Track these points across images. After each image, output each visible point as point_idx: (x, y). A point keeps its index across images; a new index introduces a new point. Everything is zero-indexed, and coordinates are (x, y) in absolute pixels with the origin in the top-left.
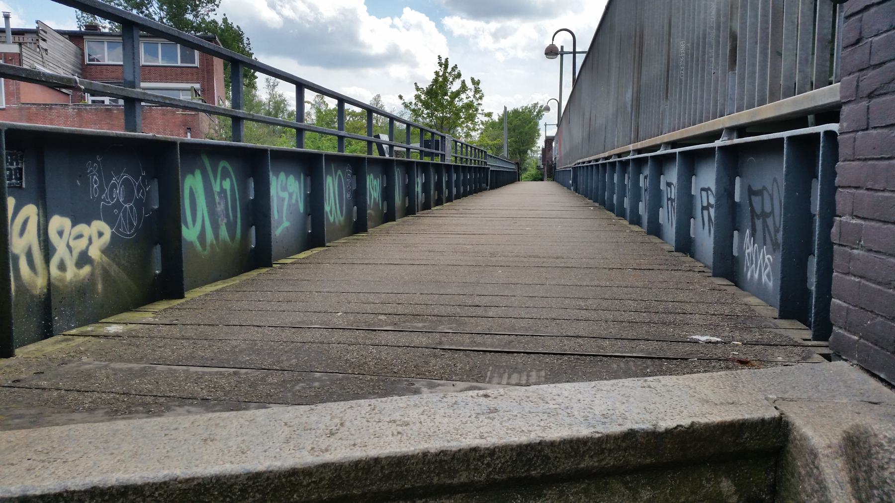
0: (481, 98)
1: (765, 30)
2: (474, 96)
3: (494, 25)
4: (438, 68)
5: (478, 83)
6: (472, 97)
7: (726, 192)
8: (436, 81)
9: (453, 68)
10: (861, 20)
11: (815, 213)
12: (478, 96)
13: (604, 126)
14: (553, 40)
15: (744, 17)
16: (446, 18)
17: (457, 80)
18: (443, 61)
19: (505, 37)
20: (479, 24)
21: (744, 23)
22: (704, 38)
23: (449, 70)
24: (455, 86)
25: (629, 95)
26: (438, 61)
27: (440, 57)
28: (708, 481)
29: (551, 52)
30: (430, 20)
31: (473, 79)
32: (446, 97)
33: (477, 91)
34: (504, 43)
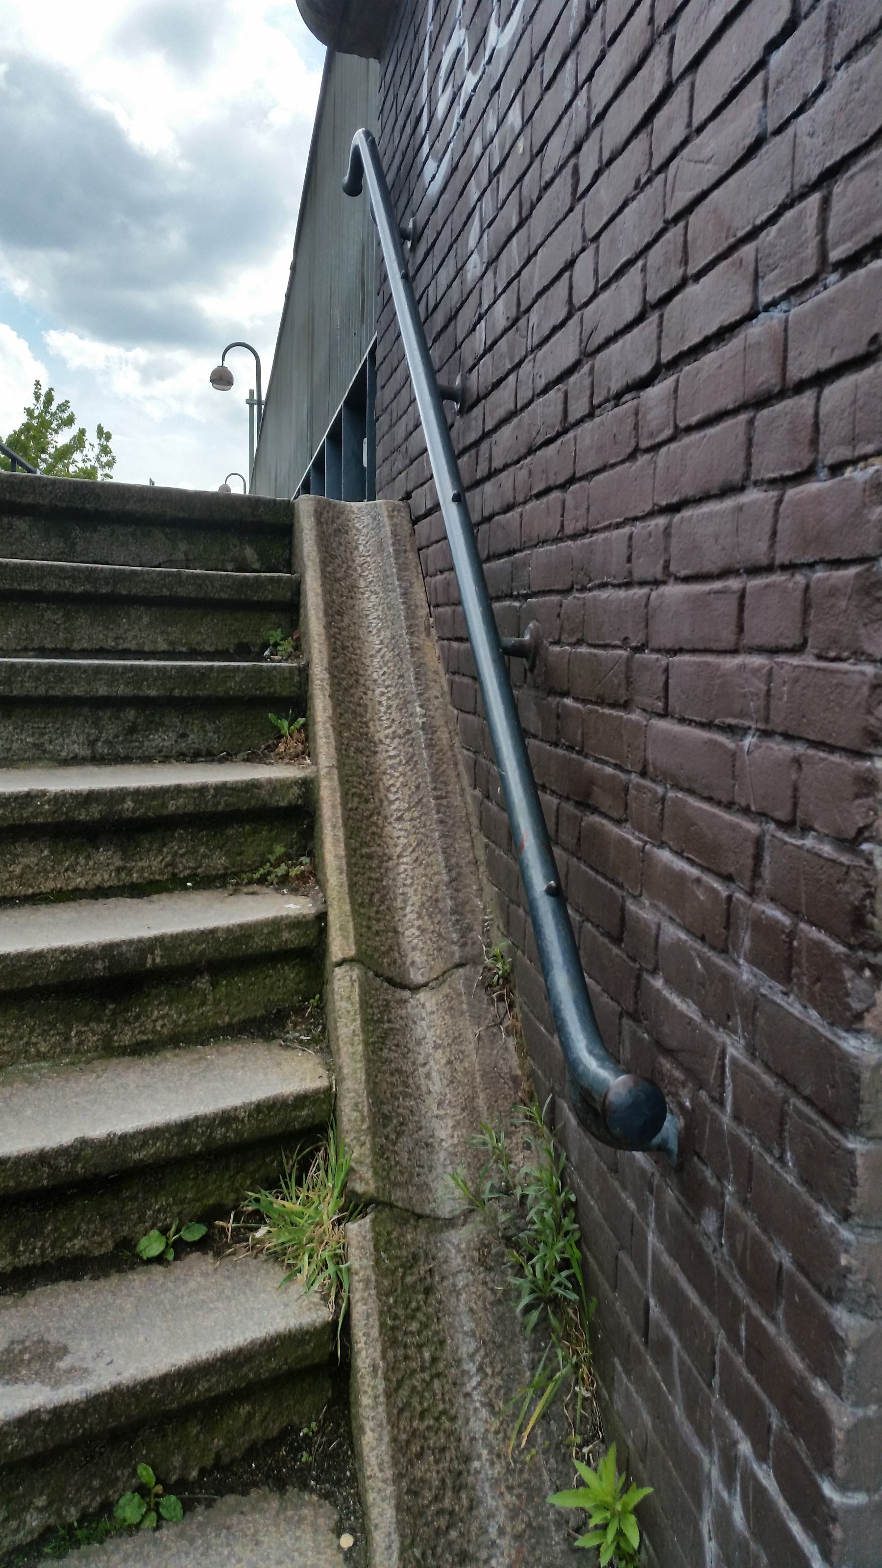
0: (110, 464)
3: (140, 354)
4: (31, 403)
5: (108, 437)
6: (93, 461)
8: (27, 428)
9: (59, 406)
10: (751, 422)
11: (509, 565)
12: (104, 459)
14: (223, 359)
16: (52, 332)
17: (66, 429)
18: (43, 391)
19: (161, 377)
20: (115, 351)
23: (53, 408)
24: (62, 438)
26: (32, 388)
27: (38, 383)
28: (235, 546)
29: (221, 379)
30: (19, 336)
31: (100, 430)
32: (43, 456)
33: (105, 450)
34: (161, 388)
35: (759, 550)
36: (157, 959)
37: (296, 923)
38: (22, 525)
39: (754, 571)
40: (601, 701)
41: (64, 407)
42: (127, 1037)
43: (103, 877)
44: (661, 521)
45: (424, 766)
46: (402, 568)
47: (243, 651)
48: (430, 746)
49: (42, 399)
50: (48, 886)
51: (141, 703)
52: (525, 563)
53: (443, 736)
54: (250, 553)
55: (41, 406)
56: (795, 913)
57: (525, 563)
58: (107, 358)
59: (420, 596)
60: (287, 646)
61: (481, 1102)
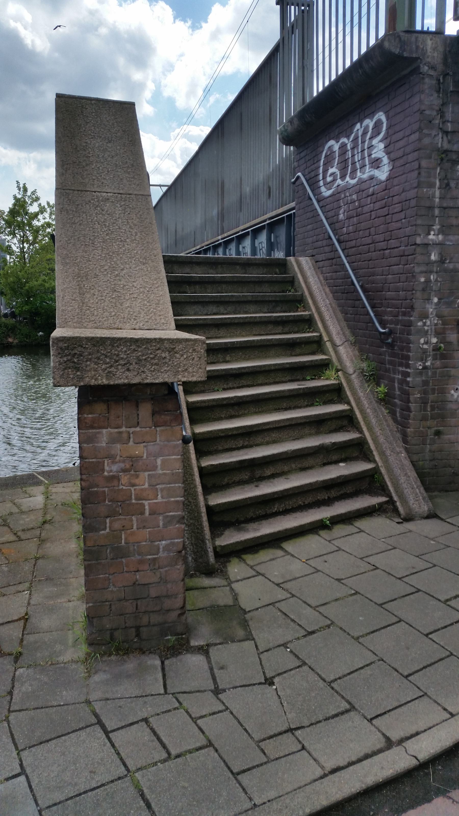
1: (279, 186)
2: (50, 218)
4: (16, 191)
6: (48, 218)
7: (269, 239)
13: (193, 233)
15: (273, 181)
18: (21, 186)
20: (23, 155)
21: (273, 183)
22: (258, 186)
23: (29, 193)
25: (215, 212)
27: (18, 182)
35: (402, 272)
36: (298, 341)
37: (317, 336)
38: (238, 267)
39: (401, 274)
40: (377, 292)
41: (34, 192)
42: (293, 354)
43: (280, 331)
44: (387, 268)
45: (331, 311)
46: (316, 273)
47: (283, 292)
48: (331, 307)
49: (22, 189)
50: (273, 332)
51: (276, 301)
52: (359, 272)
53: (334, 305)
54: (277, 270)
55: (21, 193)
56: (406, 308)
57: (359, 272)
58: (19, 159)
59: (322, 278)
60: (293, 290)
61: (354, 359)
